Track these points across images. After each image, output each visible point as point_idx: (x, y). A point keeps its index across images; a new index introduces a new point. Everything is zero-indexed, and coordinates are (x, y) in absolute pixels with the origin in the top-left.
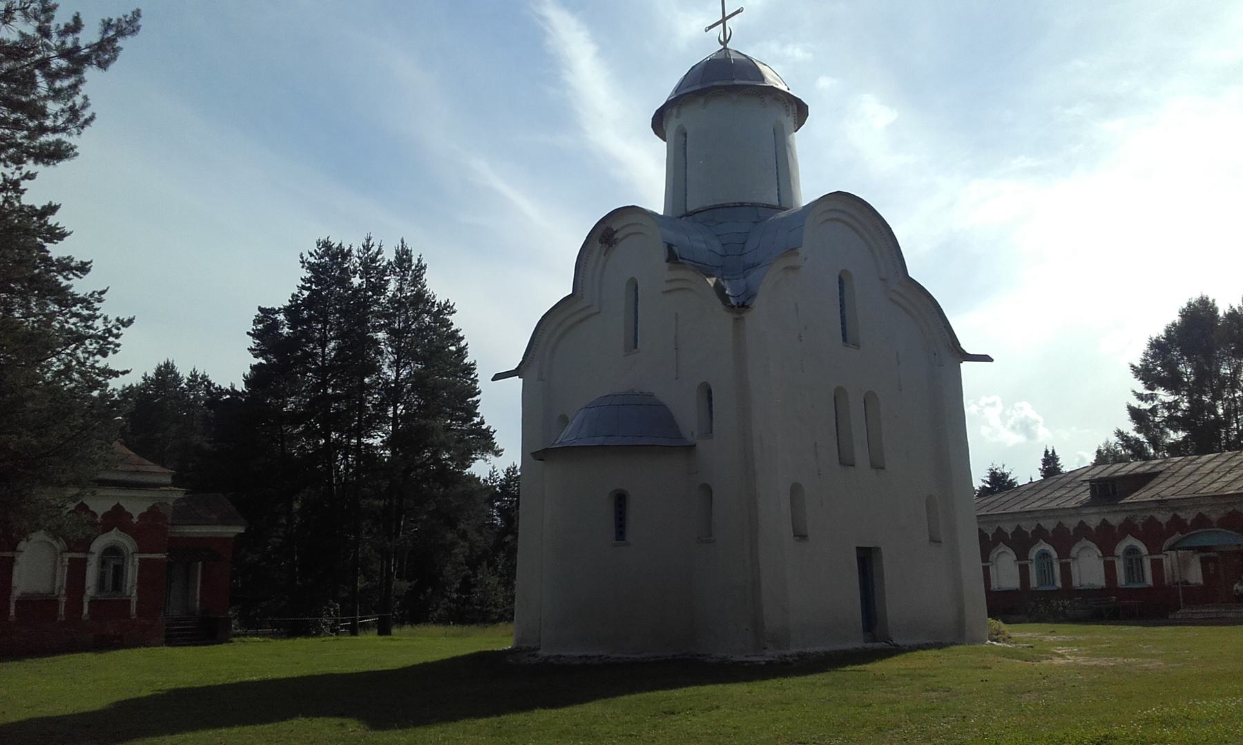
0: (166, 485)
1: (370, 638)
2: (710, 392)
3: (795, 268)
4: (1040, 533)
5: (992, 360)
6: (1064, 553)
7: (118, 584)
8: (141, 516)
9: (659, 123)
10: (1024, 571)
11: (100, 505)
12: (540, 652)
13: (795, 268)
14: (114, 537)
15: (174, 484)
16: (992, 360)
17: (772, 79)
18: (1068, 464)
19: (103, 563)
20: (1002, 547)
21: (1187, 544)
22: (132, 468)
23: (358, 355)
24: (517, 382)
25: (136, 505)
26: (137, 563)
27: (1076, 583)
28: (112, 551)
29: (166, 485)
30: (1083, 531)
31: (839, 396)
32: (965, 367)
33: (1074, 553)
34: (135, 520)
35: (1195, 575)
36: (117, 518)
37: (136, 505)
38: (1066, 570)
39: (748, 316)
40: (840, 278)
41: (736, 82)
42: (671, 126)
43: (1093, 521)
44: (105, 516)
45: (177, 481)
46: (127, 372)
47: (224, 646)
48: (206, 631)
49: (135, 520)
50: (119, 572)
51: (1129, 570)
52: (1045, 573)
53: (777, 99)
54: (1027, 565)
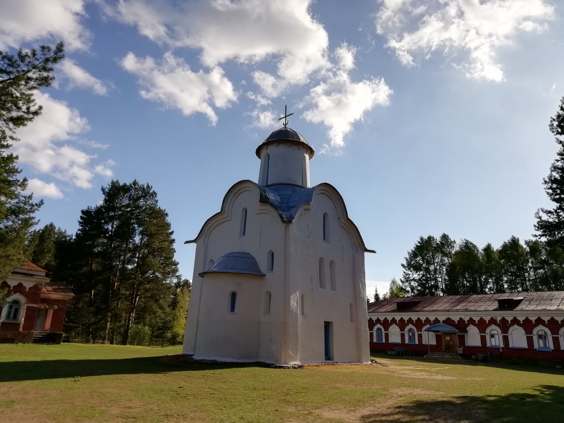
0: (43, 276)
1: (159, 348)
2: (273, 254)
3: (309, 210)
4: (539, 321)
5: (375, 252)
6: (386, 329)
7: (15, 316)
8: (30, 289)
9: (258, 152)
10: (403, 336)
11: (13, 282)
12: (193, 357)
13: (309, 210)
14: (16, 296)
15: (46, 276)
16: (375, 252)
17: (302, 140)
18: (381, 297)
19: (10, 307)
20: (394, 325)
21: (433, 329)
22: (29, 268)
23: (124, 233)
24: (194, 245)
25: (28, 284)
26: (25, 307)
27: (511, 346)
28: (16, 302)
29: (43, 276)
30: (493, 321)
31: (321, 260)
32: (366, 254)
33: (510, 331)
34: (27, 290)
35: (433, 342)
36: (19, 288)
37: (28, 284)
38: (387, 336)
39: (291, 226)
40: (244, 235)
41: (290, 139)
42: (263, 153)
43: (398, 318)
44: (15, 287)
45: (47, 275)
46: (187, 242)
47: (57, 345)
48: (51, 338)
49: (27, 290)
50: (17, 311)
51: (410, 338)
52: (411, 338)
53: (304, 147)
54: (404, 334)
